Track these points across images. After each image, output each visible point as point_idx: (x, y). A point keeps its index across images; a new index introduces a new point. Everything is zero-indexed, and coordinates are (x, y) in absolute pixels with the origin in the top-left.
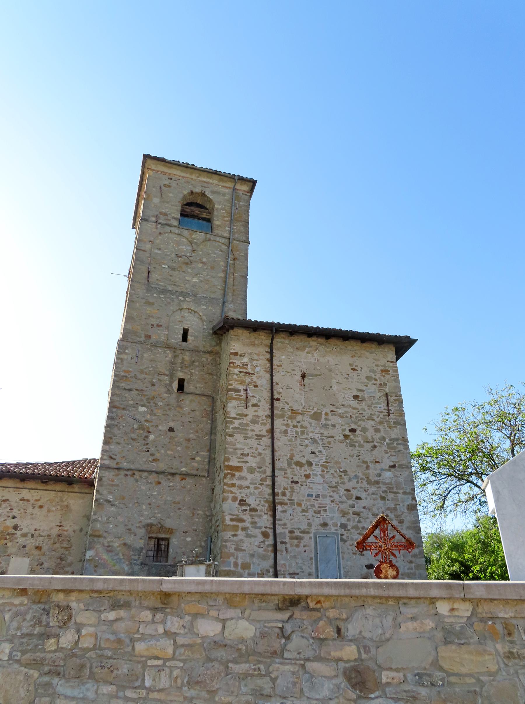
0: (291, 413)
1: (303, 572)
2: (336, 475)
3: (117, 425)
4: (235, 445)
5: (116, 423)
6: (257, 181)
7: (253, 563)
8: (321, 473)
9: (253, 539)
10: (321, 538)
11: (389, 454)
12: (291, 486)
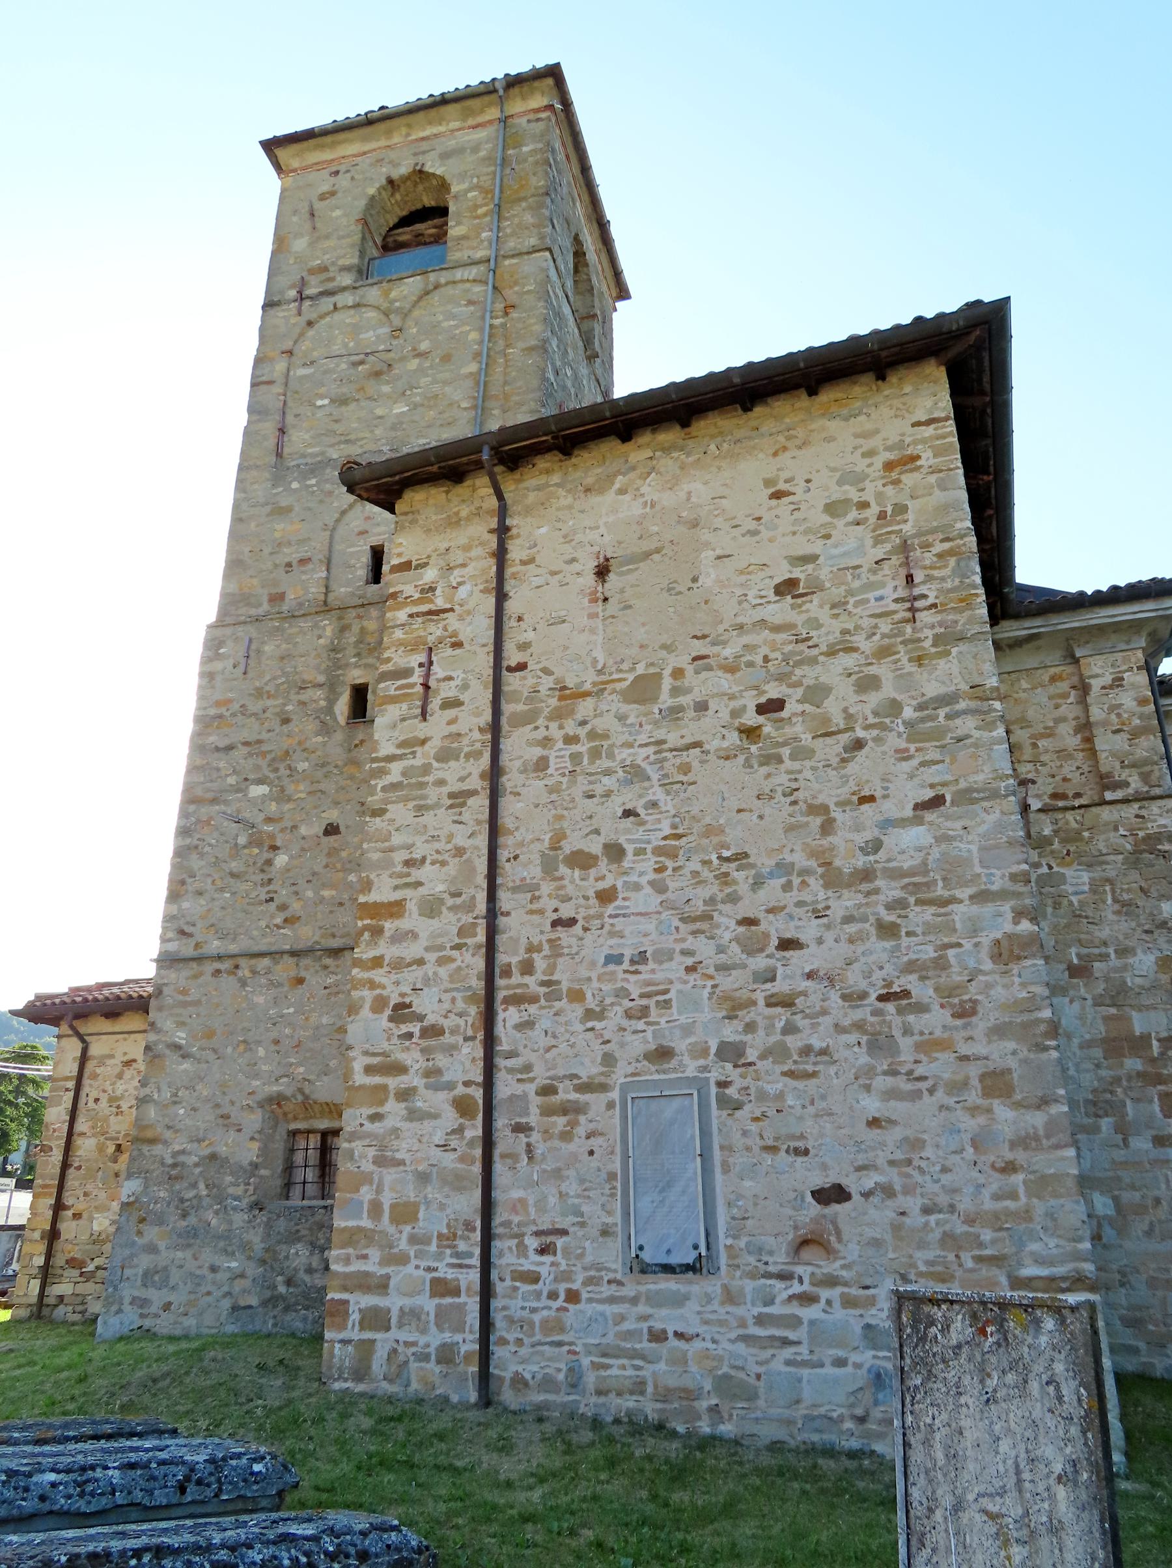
0: (561, 698)
1: (582, 1225)
2: (706, 874)
3: (196, 847)
4: (387, 838)
5: (196, 842)
6: (558, 64)
7: (428, 1203)
8: (652, 876)
9: (427, 1125)
10: (642, 1102)
11: (915, 762)
12: (553, 936)
